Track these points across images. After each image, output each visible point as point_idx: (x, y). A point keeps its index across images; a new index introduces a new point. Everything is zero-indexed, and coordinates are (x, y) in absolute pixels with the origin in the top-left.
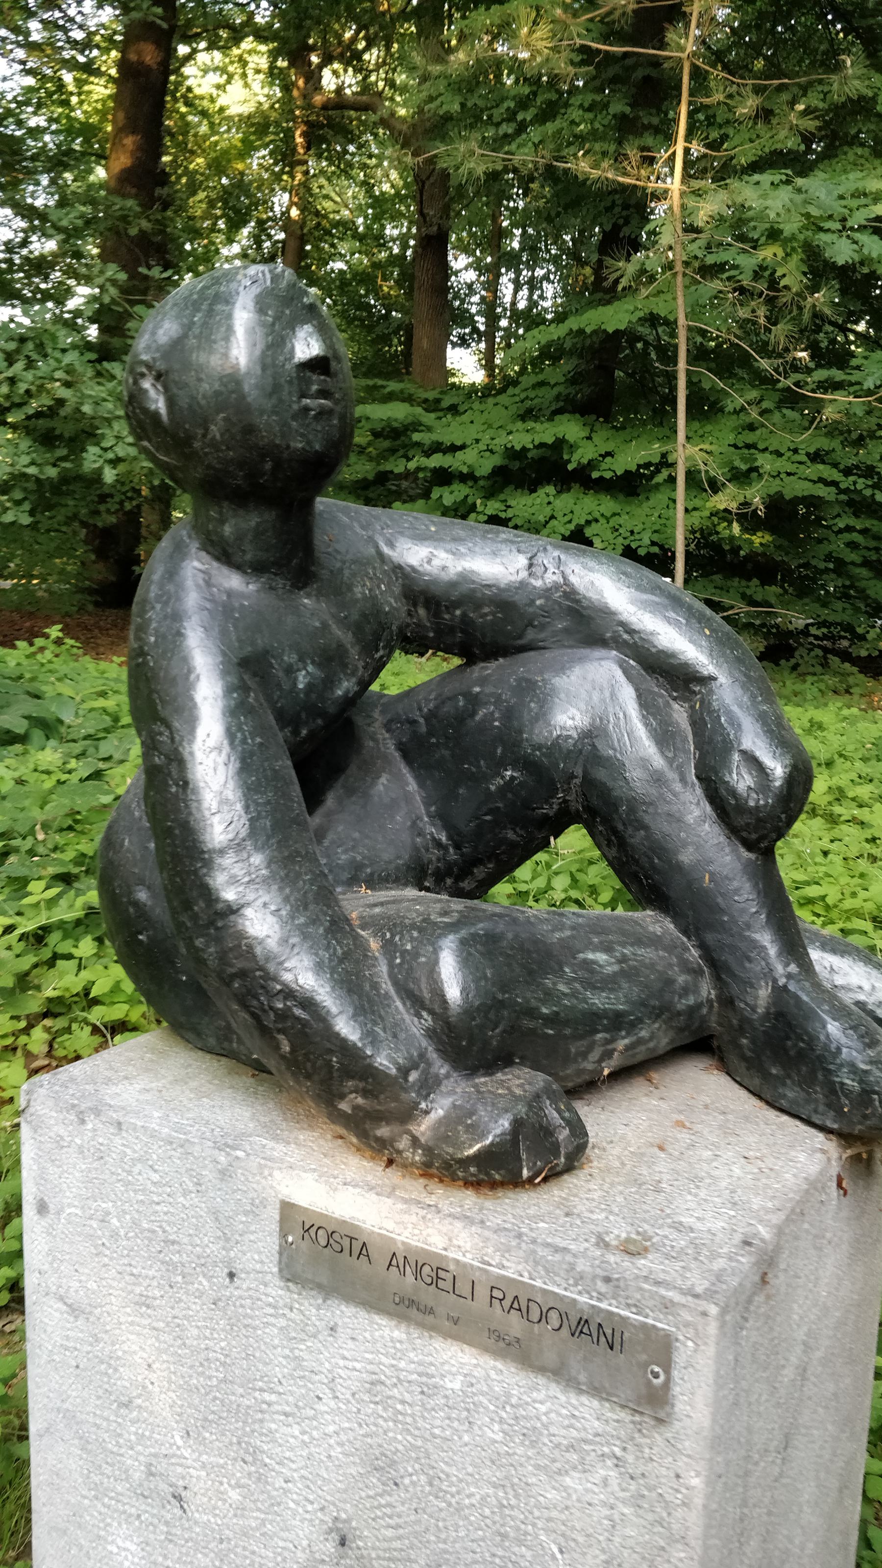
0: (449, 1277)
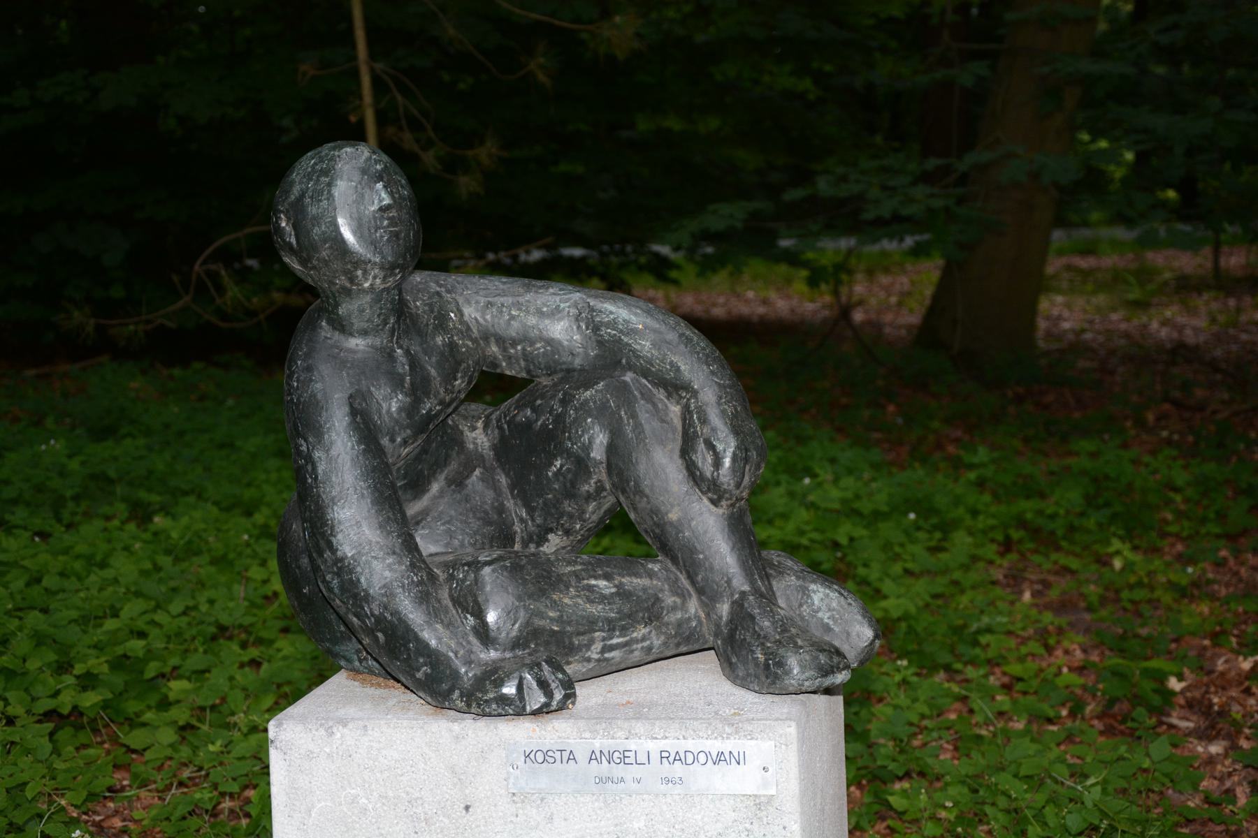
0: (631, 754)
